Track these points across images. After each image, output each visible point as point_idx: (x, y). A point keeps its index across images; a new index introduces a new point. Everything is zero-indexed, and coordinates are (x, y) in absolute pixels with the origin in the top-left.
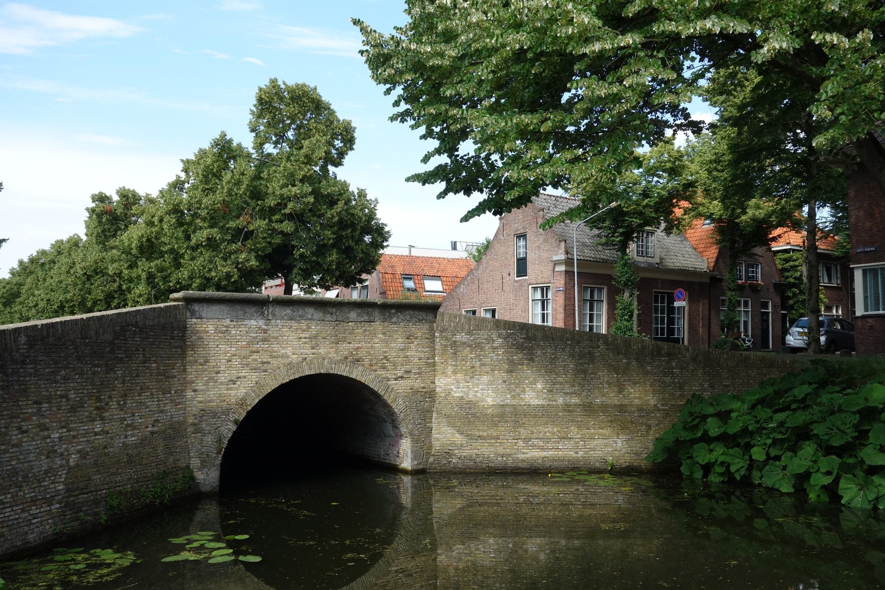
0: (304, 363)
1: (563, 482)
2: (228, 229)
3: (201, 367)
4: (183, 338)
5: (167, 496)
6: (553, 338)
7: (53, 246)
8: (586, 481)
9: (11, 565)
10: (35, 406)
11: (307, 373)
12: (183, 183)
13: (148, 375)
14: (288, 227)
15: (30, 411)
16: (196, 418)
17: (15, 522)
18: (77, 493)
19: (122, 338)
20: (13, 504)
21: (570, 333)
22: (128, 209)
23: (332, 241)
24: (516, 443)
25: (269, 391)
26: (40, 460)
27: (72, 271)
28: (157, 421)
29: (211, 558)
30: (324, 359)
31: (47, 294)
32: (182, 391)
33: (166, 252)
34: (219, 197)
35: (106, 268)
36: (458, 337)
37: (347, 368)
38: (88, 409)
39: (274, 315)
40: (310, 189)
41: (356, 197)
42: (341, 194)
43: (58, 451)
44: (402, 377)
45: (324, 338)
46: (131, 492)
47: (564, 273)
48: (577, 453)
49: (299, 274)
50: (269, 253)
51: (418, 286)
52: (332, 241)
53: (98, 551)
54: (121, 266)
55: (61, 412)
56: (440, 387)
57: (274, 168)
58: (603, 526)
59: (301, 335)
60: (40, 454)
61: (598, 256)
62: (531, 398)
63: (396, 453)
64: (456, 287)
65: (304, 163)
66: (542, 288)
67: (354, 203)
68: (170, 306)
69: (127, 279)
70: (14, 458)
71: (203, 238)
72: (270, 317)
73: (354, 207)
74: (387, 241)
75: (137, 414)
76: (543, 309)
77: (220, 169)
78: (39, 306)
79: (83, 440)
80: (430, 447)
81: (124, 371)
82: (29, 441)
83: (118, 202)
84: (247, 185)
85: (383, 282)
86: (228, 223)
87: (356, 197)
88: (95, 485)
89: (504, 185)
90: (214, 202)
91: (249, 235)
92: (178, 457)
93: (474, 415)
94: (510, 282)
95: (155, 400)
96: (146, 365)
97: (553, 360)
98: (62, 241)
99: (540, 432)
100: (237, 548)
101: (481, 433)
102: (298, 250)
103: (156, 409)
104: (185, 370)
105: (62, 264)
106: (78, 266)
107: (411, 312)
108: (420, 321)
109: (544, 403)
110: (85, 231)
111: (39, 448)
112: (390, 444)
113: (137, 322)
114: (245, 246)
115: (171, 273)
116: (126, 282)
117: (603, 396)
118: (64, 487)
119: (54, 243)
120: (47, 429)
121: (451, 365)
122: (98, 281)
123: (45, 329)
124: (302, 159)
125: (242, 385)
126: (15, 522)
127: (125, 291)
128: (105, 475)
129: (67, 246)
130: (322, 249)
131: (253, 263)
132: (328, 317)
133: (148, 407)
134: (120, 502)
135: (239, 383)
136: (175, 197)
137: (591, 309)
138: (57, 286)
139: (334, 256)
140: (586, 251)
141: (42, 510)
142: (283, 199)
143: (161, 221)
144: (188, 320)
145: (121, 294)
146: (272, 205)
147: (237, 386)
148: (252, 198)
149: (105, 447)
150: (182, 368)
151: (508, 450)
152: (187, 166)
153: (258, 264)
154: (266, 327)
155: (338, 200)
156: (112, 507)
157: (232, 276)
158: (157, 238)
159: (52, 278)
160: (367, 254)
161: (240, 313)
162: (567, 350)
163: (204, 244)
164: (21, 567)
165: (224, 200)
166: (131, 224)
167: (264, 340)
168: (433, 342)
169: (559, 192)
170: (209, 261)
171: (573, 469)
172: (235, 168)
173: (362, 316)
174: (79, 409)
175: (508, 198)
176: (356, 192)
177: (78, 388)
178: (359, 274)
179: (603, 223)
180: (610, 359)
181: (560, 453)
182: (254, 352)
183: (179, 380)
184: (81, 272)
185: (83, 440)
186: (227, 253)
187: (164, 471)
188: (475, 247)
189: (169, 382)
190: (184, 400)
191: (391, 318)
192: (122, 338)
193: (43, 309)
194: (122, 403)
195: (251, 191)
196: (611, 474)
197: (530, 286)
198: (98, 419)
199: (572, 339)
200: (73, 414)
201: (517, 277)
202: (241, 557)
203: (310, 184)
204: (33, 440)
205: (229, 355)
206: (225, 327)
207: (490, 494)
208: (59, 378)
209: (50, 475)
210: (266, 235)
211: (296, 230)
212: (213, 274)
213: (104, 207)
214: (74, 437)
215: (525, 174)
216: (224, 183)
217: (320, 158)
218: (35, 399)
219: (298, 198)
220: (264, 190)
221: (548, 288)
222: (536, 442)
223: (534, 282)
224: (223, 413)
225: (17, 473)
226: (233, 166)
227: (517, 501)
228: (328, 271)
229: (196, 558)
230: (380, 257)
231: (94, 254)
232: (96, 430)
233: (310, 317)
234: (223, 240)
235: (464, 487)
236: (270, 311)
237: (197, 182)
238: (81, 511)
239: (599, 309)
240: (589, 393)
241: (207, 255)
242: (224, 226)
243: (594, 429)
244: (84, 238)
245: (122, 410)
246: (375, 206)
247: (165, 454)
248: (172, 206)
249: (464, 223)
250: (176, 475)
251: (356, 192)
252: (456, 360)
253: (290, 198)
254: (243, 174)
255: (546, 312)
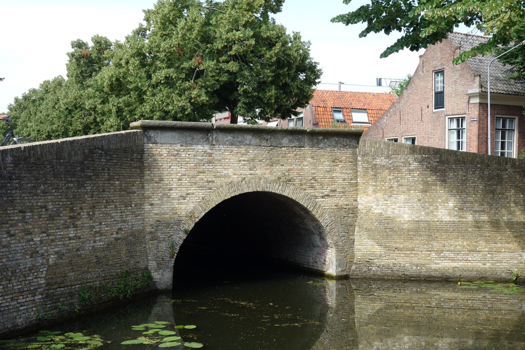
0: (243, 182)
1: (469, 290)
2: (183, 69)
3: (156, 185)
4: (141, 160)
5: (129, 292)
6: (464, 162)
7: (42, 86)
8: (492, 289)
9: (3, 343)
10: (21, 214)
11: (246, 191)
12: (145, 30)
13: (112, 190)
14: (233, 66)
15: (16, 218)
16: (152, 228)
17: (6, 309)
18: (55, 287)
19: (90, 159)
20: (4, 294)
21: (480, 157)
22: (101, 54)
23: (270, 79)
24: (429, 254)
25: (214, 205)
26: (26, 259)
27: (57, 107)
28: (120, 229)
29: (161, 343)
30: (260, 179)
31: (37, 125)
32: (141, 205)
33: (132, 90)
34: (175, 41)
35: (83, 104)
36: (378, 161)
37: (281, 187)
38: (64, 218)
39: (217, 141)
40: (252, 33)
41: (292, 40)
42: (279, 37)
43: (40, 251)
44: (328, 196)
45: (260, 161)
46: (100, 288)
47: (478, 104)
48: (484, 264)
49: (243, 108)
50: (217, 90)
51: (346, 117)
52: (270, 79)
53: (71, 334)
54: (95, 102)
55: (41, 219)
56: (362, 204)
57: (221, 15)
58: (386, 277)
59: (241, 158)
60: (25, 254)
61: (510, 89)
62: (443, 215)
63: (323, 261)
64: (380, 118)
65: (246, 10)
66: (458, 119)
67: (290, 45)
68: (130, 133)
69: (101, 113)
70: (4, 256)
71: (161, 77)
72: (214, 143)
73: (290, 49)
74: (319, 78)
75: (103, 223)
76: (459, 138)
77: (176, 17)
78: (31, 136)
79: (59, 243)
80: (353, 257)
81: (93, 187)
82: (16, 243)
83: (93, 48)
84: (198, 31)
85: (316, 114)
86: (182, 64)
87: (292, 40)
88: (70, 281)
89: (421, 23)
90: (170, 45)
91: (200, 74)
92: (138, 260)
93: (392, 230)
94: (428, 114)
95: (119, 211)
96: (110, 182)
97: (464, 182)
98: (49, 82)
99: (451, 245)
100: (185, 336)
101: (398, 245)
102: (242, 86)
103: (120, 219)
104: (143, 187)
105: (49, 101)
106: (61, 102)
107: (337, 139)
108: (344, 146)
109: (455, 220)
110: (66, 72)
111: (24, 249)
112: (318, 253)
113: (102, 146)
114: (197, 83)
115: (136, 108)
116: (100, 115)
117: (510, 214)
118: (45, 282)
119: (42, 83)
120: (31, 234)
121: (372, 185)
122: (77, 114)
123: (27, 151)
124: (245, 6)
125: (191, 201)
126: (6, 309)
127: (99, 122)
128: (78, 273)
129: (53, 85)
130: (262, 86)
131: (204, 98)
132: (264, 143)
133: (112, 218)
134: (90, 295)
135: (188, 198)
136: (138, 42)
137: (503, 137)
138: (45, 119)
139: (272, 92)
140: (499, 85)
141: (27, 299)
142: (229, 42)
143: (127, 63)
144: (145, 145)
145: (96, 126)
146: (220, 47)
147: (186, 201)
148: (202, 42)
149: (78, 250)
150: (141, 185)
151: (422, 261)
152: (148, 16)
153: (207, 99)
154: (210, 151)
155: (276, 42)
156: (84, 299)
157: (186, 110)
158: (124, 78)
159: (41, 112)
160: (301, 90)
161: (189, 139)
162: (477, 172)
163: (162, 82)
164: (12, 344)
165: (179, 44)
166: (103, 66)
167: (209, 162)
168: (356, 165)
169: (473, 30)
170: (167, 96)
171: (481, 278)
172: (188, 16)
173: (293, 142)
174: (56, 218)
175: (423, 35)
176: (292, 35)
177: (54, 200)
178: (295, 107)
179: (516, 59)
180: (517, 180)
181: (469, 264)
182: (201, 172)
183: (138, 195)
184: (64, 107)
185: (59, 243)
186: (182, 89)
187: (127, 271)
188: (398, 83)
189: (130, 197)
190: (143, 212)
191: (319, 144)
192: (90, 159)
193: (35, 138)
194: (91, 213)
195: (202, 36)
196: (516, 284)
197: (447, 117)
198: (72, 226)
199: (482, 163)
200: (51, 222)
201: (435, 109)
202: (186, 343)
203: (251, 29)
204: (20, 242)
205: (180, 174)
206: (176, 150)
207: (405, 299)
208: (39, 191)
209: (33, 271)
210: (214, 74)
211: (241, 69)
212: (170, 108)
213: (81, 52)
214: (52, 241)
215: (439, 12)
216: (179, 29)
217: (260, 6)
218: (20, 208)
219: (242, 41)
220: (213, 34)
221: (463, 119)
222: (447, 254)
223: (450, 113)
224: (175, 224)
225: (7, 269)
226: (186, 15)
227: (429, 305)
228: (268, 105)
229: (149, 343)
230: (313, 92)
231: (74, 92)
232: (70, 235)
233: (248, 142)
234: (178, 79)
235: (383, 292)
236: (214, 137)
237: (157, 29)
238: (59, 301)
239: (511, 138)
240: (497, 212)
241: (165, 91)
242: (179, 66)
243: (501, 243)
244: (66, 78)
245: (91, 219)
246: (309, 47)
247: (127, 257)
248: (136, 50)
249: (384, 59)
250: (137, 274)
251: (292, 35)
252: (376, 181)
253: (234, 41)
254: (194, 21)
255: (461, 140)
